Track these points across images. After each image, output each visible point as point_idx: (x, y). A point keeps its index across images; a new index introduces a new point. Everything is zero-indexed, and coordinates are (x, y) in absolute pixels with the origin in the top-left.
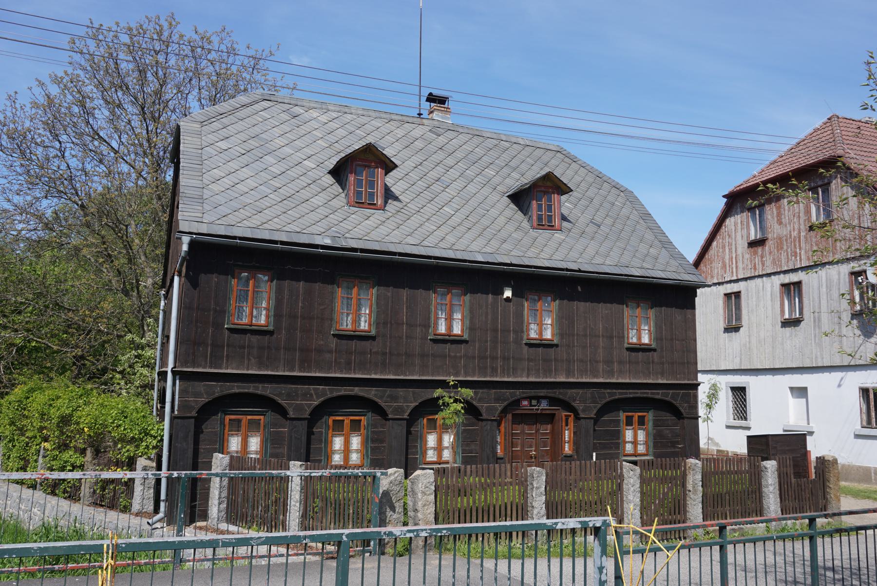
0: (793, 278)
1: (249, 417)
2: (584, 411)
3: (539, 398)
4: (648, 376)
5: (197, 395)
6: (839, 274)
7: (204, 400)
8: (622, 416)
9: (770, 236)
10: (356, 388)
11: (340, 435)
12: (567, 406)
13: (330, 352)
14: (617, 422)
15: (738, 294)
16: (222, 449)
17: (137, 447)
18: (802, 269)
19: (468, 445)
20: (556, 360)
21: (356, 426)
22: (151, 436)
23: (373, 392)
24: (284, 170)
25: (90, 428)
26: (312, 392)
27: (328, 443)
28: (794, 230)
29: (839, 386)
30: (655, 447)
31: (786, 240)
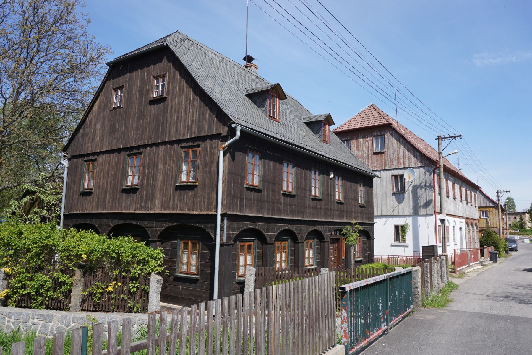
13: (281, 204)
27: (274, 257)
29: (385, 224)
30: (363, 254)
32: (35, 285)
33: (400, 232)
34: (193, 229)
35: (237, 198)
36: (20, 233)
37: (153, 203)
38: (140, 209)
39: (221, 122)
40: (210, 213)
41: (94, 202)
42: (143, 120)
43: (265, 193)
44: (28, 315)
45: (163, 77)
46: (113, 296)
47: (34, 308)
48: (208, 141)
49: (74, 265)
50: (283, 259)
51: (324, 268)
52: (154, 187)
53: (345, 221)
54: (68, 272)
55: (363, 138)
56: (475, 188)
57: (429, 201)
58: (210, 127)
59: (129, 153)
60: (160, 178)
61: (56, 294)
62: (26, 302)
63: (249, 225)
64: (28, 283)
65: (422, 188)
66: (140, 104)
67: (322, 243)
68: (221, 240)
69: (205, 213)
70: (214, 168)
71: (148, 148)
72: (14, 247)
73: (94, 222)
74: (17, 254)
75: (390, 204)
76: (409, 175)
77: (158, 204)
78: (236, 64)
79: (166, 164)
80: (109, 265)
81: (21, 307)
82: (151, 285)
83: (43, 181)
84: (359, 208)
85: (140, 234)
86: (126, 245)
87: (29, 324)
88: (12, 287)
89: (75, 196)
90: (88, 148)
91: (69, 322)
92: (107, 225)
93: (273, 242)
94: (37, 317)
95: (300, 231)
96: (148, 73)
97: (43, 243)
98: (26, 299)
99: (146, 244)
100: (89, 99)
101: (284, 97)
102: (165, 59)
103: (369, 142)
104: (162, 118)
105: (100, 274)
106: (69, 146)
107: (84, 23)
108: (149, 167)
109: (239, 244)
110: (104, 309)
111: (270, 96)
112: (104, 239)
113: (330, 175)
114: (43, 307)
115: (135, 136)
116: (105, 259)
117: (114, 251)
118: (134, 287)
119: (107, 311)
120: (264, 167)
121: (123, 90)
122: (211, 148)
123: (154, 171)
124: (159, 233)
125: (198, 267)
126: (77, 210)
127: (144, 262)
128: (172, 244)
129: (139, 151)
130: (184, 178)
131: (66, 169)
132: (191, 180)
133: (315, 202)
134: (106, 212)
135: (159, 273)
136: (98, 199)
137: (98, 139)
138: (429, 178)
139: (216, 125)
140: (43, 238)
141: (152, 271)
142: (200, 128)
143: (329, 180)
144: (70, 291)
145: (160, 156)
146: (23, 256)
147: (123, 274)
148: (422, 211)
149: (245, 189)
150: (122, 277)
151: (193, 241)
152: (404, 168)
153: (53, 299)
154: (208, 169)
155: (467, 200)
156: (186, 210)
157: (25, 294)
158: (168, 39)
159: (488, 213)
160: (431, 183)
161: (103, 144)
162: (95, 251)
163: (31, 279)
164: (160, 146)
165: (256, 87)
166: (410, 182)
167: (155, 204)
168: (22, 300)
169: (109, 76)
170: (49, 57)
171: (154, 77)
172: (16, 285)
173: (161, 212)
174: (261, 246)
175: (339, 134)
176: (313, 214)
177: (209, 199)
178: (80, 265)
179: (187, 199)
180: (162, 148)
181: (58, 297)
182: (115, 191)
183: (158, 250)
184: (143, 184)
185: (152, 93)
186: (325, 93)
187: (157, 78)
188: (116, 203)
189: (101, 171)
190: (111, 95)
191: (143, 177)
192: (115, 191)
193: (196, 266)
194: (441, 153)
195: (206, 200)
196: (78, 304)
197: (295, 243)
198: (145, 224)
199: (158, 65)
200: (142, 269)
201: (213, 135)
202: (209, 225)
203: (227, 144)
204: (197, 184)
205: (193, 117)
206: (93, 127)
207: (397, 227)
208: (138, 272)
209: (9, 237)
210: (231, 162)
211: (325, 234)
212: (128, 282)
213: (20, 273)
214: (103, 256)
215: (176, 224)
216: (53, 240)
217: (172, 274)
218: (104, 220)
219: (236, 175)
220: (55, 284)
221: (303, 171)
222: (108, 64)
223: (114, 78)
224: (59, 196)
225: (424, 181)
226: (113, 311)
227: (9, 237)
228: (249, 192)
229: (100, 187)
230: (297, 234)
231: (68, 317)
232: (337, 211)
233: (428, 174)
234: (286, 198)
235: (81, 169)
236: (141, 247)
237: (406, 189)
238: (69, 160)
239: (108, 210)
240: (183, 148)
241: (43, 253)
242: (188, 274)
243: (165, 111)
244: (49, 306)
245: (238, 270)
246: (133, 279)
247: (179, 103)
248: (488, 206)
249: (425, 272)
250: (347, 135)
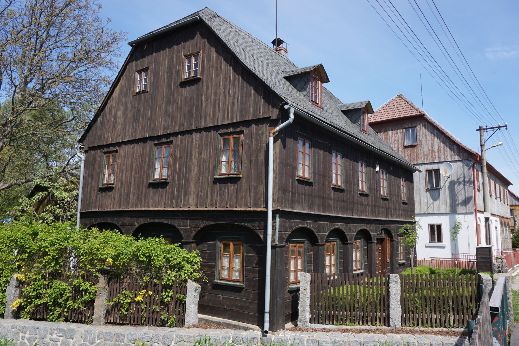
13: (331, 199)
27: (324, 261)
32: (52, 294)
33: (436, 232)
34: (239, 229)
35: (289, 192)
36: (35, 234)
37: (187, 199)
38: (171, 205)
39: (269, 104)
40: (259, 209)
41: (116, 198)
42: (173, 105)
43: (315, 187)
44: (46, 330)
45: (196, 55)
46: (143, 306)
47: (51, 321)
48: (254, 126)
49: (98, 271)
50: (333, 263)
51: (394, 274)
52: (187, 180)
54: (90, 278)
55: (392, 130)
56: (506, 183)
57: (468, 198)
58: (256, 111)
59: (156, 142)
60: (195, 170)
61: (77, 305)
62: (42, 314)
63: (301, 224)
64: (44, 291)
65: (460, 183)
66: (169, 87)
67: (369, 244)
68: (273, 241)
69: (252, 209)
70: (262, 157)
71: (179, 136)
72: (28, 250)
73: (115, 221)
74: (31, 258)
75: (424, 201)
76: (445, 169)
77: (192, 199)
78: (267, 47)
79: (201, 153)
80: (138, 271)
81: (36, 319)
82: (188, 294)
83: (56, 176)
84: (402, 205)
85: (173, 236)
86: (157, 247)
87: (47, 340)
88: (25, 297)
89: (93, 192)
90: (107, 138)
91: (94, 338)
92: (132, 224)
93: (324, 243)
94: (56, 332)
95: (350, 230)
96: (178, 52)
97: (61, 245)
98: (41, 310)
99: (180, 246)
100: (105, 89)
101: (326, 80)
102: (198, 35)
103: (399, 134)
104: (195, 101)
105: (127, 281)
106: (86, 137)
107: (96, 8)
108: (180, 158)
109: (291, 247)
110: (132, 322)
111: (312, 79)
112: (131, 240)
113: (375, 168)
114: (62, 319)
115: (163, 123)
116: (133, 263)
117: (144, 255)
118: (168, 296)
119: (135, 325)
120: (314, 156)
121: (149, 72)
122: (257, 134)
123: (186, 163)
124: (194, 233)
125: (243, 273)
126: (95, 208)
127: (179, 267)
128: (210, 246)
129: (169, 140)
130: (224, 170)
131: (83, 162)
132: (232, 172)
133: (363, 198)
134: (130, 209)
135: (196, 280)
136: (121, 195)
137: (119, 127)
138: (469, 173)
139: (264, 108)
140: (62, 239)
141: (189, 278)
142: (242, 111)
143: (375, 173)
144: (93, 301)
145: (194, 145)
146: (39, 260)
147: (155, 281)
148: (461, 209)
149: (296, 182)
150: (153, 284)
151: (236, 243)
152: (440, 162)
153: (72, 310)
154: (253, 158)
155: (500, 198)
156: (228, 206)
157: (41, 305)
158: (200, 13)
159: (514, 211)
160: (470, 178)
161: (125, 133)
162: (123, 254)
163: (48, 287)
164: (194, 134)
165: (290, 71)
166: (446, 179)
167: (189, 200)
168: (37, 311)
169: (132, 58)
170: (59, 44)
171: (185, 56)
172: (30, 294)
173: (196, 209)
174: (311, 247)
175: (372, 125)
176: (361, 211)
177: (256, 193)
178: (105, 270)
179: (228, 193)
180: (196, 136)
181: (79, 307)
182: (141, 186)
183: (194, 253)
184: (174, 178)
185: (183, 74)
186: (362, 80)
187: (189, 57)
188: (141, 199)
189: (124, 163)
190: (134, 78)
191: (174, 170)
192: (141, 186)
193: (239, 271)
194: (484, 145)
195: (253, 195)
196: (103, 316)
197: (343, 244)
198: (177, 223)
199: (190, 43)
200: (176, 275)
201: (260, 119)
202: (257, 224)
203: (278, 128)
204: (241, 176)
205: (234, 99)
206: (113, 114)
207: (432, 227)
208: (173, 278)
209: (22, 238)
210: (283, 149)
211: (372, 234)
212: (160, 290)
213: (35, 280)
214: (130, 260)
215: (215, 223)
216: (73, 241)
217: (210, 281)
218: (128, 219)
219: (287, 165)
220: (75, 293)
221: (351, 162)
222: (130, 44)
223: (136, 60)
224: (75, 193)
225: (462, 176)
226: (143, 325)
227: (22, 238)
228: (301, 186)
229: (122, 182)
230: (346, 234)
231: (93, 333)
232: (383, 208)
233: (467, 168)
234: (336, 193)
235: (100, 162)
236: (175, 249)
237: (442, 185)
238: (86, 152)
239: (132, 207)
240: (221, 135)
241: (62, 256)
242: (229, 281)
243: (199, 94)
244: (69, 318)
245: (289, 276)
246: (167, 287)
247: (216, 84)
248: (514, 204)
250: (380, 126)
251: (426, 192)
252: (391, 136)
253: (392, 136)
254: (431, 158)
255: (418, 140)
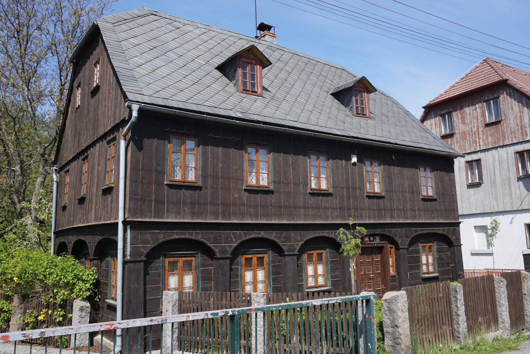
0: (475, 157)
1: (184, 259)
2: (401, 244)
3: (374, 235)
4: (433, 218)
5: (146, 242)
6: (507, 153)
7: (150, 246)
8: (420, 245)
9: (456, 131)
10: (263, 232)
11: (188, 274)
12: (392, 241)
14: (418, 252)
15: (478, 161)
16: (323, 276)
17: (72, 291)
18: (481, 151)
19: (334, 272)
20: (384, 209)
21: (188, 267)
22: (83, 281)
23: (274, 235)
24: (185, 64)
25: (20, 277)
26: (232, 236)
27: (243, 277)
28: (474, 127)
29: (511, 223)
30: (439, 267)
31: (469, 134)
53: (388, 221)
55: (469, 106)
68: (124, 256)
103: (478, 110)
230: (280, 244)
242: (317, 288)
249: (453, 299)
251: (518, 181)
252: (468, 113)
253: (470, 113)
254: (520, 136)
255: (502, 113)
